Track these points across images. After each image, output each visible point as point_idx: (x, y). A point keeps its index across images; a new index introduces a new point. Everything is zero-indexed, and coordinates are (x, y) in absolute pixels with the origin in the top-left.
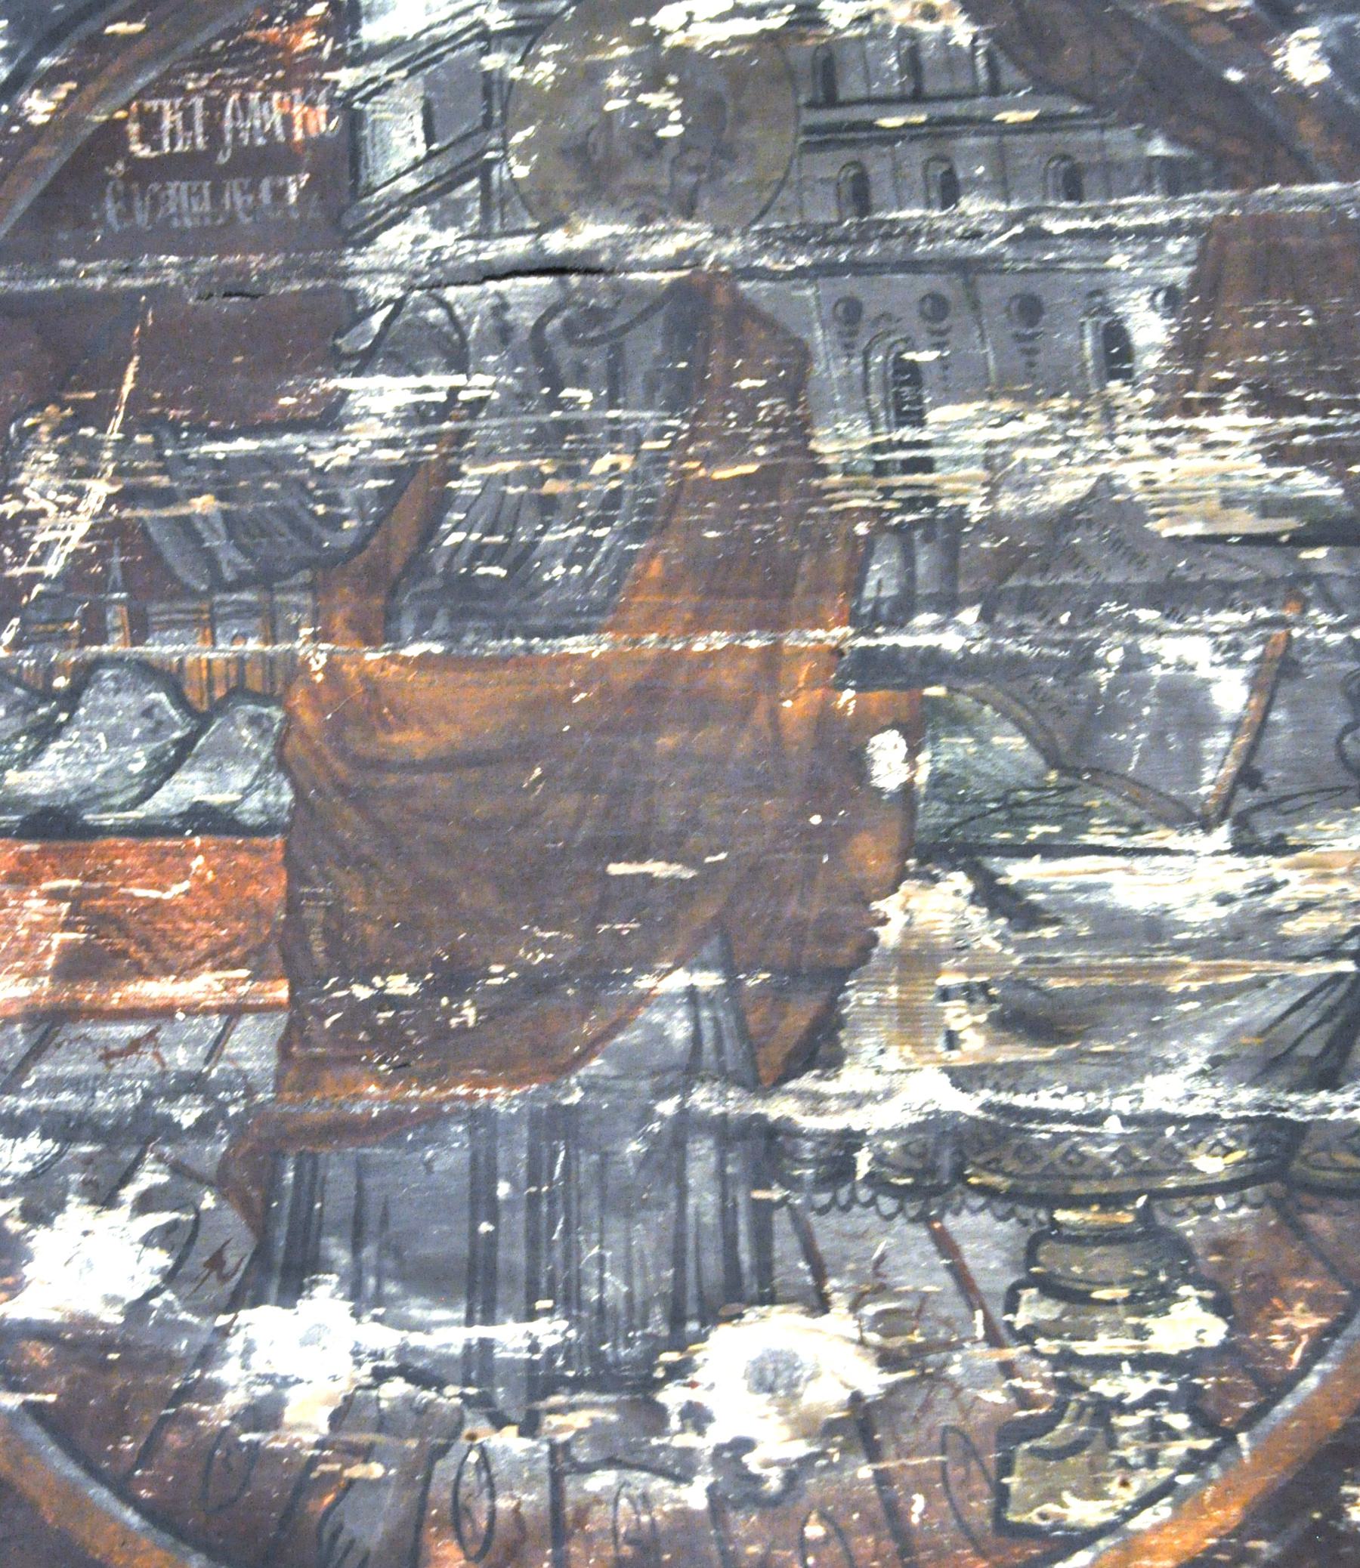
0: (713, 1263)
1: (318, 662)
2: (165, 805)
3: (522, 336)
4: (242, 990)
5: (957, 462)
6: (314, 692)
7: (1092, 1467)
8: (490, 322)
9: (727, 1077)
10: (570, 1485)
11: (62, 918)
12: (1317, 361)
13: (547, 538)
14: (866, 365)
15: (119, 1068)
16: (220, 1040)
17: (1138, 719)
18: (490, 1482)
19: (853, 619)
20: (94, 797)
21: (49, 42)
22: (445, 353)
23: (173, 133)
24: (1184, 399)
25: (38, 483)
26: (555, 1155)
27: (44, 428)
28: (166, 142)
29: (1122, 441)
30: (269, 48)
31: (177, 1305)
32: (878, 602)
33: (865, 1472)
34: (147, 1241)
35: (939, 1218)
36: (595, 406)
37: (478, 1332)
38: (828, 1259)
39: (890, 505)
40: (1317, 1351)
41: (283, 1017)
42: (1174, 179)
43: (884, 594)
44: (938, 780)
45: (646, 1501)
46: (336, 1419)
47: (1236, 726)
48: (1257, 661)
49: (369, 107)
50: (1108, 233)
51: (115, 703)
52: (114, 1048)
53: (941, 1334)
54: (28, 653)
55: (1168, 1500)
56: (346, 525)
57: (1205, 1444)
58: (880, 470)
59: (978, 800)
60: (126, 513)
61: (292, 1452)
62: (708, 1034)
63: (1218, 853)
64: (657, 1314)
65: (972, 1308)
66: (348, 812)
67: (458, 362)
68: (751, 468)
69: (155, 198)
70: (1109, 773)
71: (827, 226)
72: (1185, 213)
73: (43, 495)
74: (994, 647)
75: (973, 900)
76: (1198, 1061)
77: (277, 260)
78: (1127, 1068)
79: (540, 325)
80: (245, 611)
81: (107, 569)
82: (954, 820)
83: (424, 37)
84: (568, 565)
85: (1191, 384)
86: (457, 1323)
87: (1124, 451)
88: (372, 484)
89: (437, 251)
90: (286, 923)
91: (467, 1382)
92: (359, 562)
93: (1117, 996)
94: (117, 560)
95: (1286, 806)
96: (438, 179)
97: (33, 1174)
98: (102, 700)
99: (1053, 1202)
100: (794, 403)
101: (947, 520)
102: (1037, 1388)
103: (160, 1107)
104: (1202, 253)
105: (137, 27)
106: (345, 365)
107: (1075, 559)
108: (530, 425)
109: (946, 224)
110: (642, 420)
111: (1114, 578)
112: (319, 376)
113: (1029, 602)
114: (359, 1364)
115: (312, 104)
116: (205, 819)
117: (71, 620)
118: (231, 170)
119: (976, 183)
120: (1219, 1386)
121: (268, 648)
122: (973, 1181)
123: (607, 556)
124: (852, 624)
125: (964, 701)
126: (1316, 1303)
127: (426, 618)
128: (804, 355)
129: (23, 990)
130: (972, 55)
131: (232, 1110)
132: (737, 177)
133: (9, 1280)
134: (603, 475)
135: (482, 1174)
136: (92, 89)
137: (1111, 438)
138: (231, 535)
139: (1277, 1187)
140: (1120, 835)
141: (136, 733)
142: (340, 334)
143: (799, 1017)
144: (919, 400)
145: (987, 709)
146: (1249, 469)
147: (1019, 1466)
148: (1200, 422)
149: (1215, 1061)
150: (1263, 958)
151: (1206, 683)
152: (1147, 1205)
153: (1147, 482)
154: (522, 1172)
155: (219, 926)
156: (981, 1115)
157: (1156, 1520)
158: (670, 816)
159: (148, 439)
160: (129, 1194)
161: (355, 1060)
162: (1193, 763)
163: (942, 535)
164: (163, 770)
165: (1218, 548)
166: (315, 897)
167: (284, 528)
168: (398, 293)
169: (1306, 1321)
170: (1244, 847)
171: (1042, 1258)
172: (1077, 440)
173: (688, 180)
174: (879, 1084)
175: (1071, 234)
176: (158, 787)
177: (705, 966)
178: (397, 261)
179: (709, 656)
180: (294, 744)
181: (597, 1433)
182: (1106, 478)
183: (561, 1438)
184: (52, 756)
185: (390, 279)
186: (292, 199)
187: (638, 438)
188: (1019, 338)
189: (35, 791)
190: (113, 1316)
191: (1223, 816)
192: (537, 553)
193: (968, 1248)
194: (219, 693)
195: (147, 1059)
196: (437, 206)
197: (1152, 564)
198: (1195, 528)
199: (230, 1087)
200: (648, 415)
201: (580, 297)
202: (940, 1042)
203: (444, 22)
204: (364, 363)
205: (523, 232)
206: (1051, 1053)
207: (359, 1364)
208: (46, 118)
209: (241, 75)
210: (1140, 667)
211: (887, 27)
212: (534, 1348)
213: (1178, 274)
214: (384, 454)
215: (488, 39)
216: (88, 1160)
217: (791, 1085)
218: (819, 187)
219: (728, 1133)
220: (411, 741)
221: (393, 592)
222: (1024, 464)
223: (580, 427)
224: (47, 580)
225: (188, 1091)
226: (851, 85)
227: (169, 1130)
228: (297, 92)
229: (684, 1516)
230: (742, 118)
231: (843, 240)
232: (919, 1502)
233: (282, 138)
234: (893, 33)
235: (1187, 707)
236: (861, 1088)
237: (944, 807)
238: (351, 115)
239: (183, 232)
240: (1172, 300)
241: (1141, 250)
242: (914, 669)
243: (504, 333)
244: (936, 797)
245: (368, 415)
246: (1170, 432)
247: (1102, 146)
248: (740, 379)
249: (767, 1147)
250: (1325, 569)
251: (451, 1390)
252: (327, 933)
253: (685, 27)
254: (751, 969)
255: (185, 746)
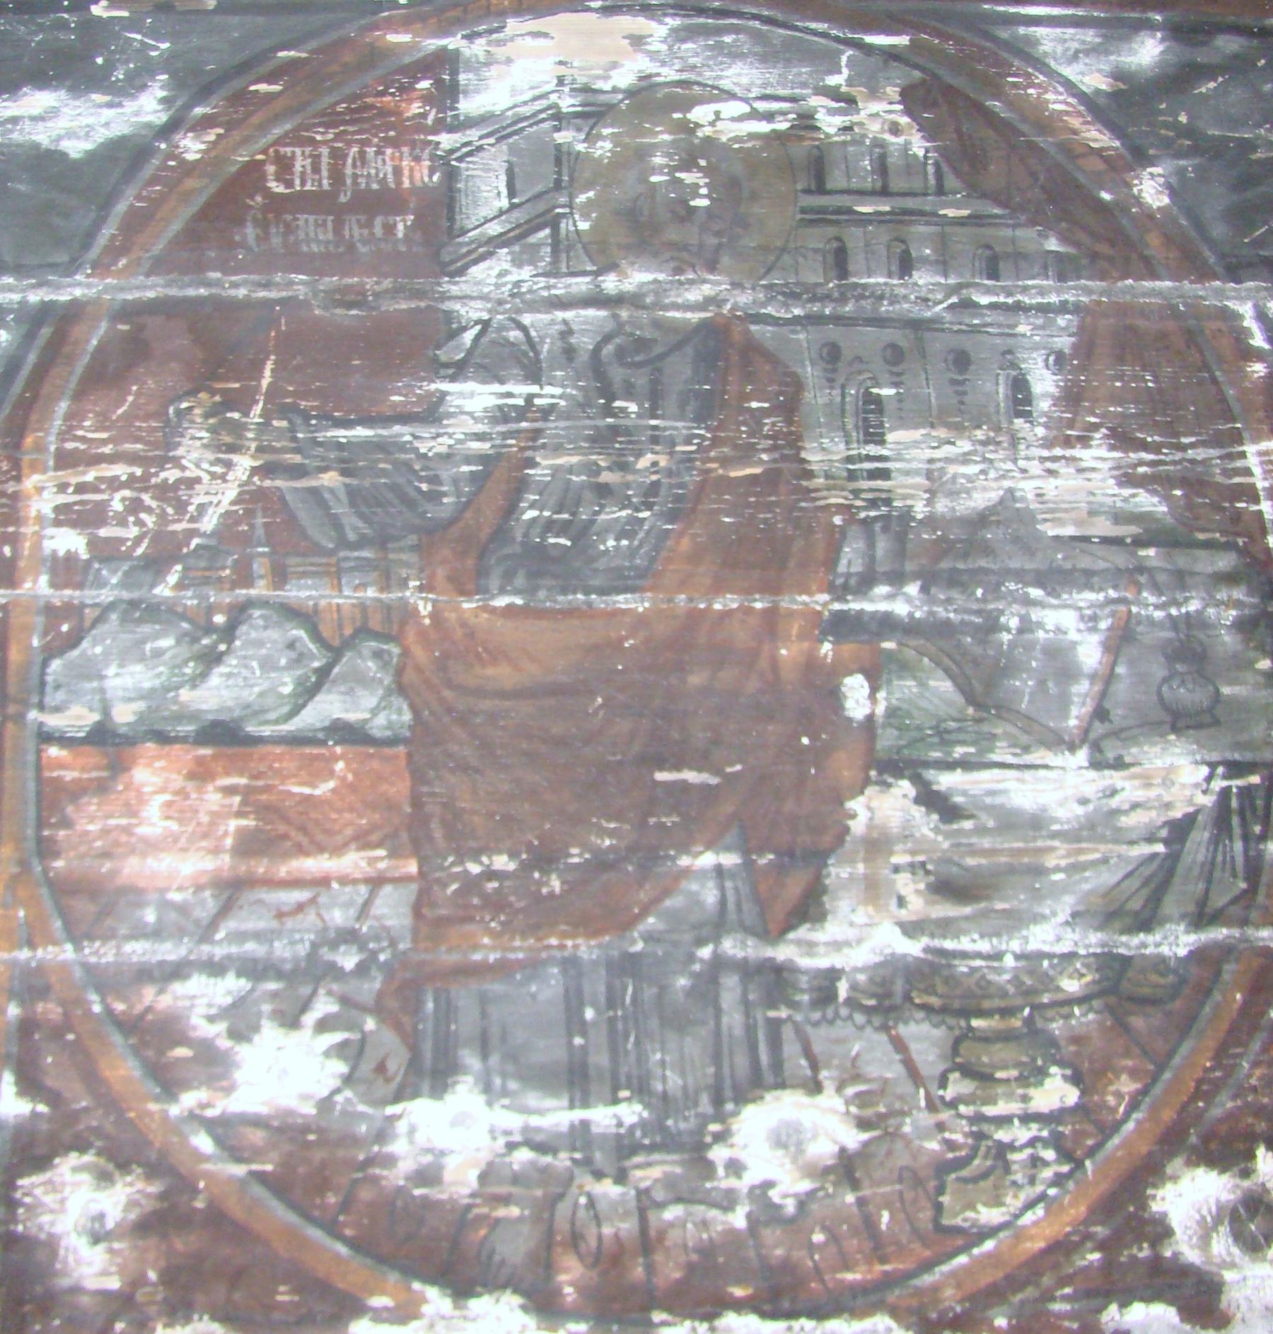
0: (742, 1062)
1: (425, 609)
2: (310, 721)
3: (583, 358)
4: (382, 865)
5: (907, 473)
6: (422, 633)
7: (996, 1187)
8: (559, 344)
9: (749, 931)
10: (652, 1216)
11: (235, 808)
12: (1155, 413)
13: (603, 517)
14: (843, 396)
15: (290, 923)
16: (367, 904)
17: (1029, 670)
18: (596, 1217)
19: (830, 588)
20: (257, 713)
21: (204, 93)
22: (523, 367)
23: (303, 174)
24: (1067, 436)
25: (195, 455)
26: (625, 989)
27: (197, 411)
28: (298, 182)
29: (1021, 463)
30: (384, 112)
31: (355, 1100)
32: (848, 575)
33: (850, 1198)
34: (327, 1054)
35: (895, 1027)
36: (639, 415)
37: (578, 1114)
38: (820, 1058)
39: (858, 503)
40: (1133, 1106)
41: (414, 887)
42: (1063, 269)
43: (853, 570)
44: (892, 712)
45: (705, 1224)
46: (483, 1178)
47: (1093, 677)
48: (1109, 629)
49: (463, 165)
50: (1018, 307)
51: (262, 635)
52: (285, 909)
53: (897, 1106)
54: (190, 593)
55: (1042, 1205)
56: (445, 500)
57: (1065, 1168)
58: (852, 476)
59: (919, 728)
60: (267, 483)
61: (451, 1200)
62: (731, 899)
63: (1081, 768)
64: (705, 1099)
65: (917, 1088)
66: (456, 730)
67: (534, 374)
68: (757, 470)
69: (287, 226)
70: (1009, 710)
71: (817, 285)
72: (1070, 297)
73: (198, 466)
74: (931, 613)
75: (917, 801)
76: (1063, 916)
77: (387, 283)
78: (1016, 920)
79: (596, 351)
80: (363, 566)
81: (252, 526)
82: (902, 743)
83: (510, 113)
84: (617, 539)
85: (1071, 424)
86: (562, 1109)
87: (1024, 471)
88: (465, 469)
89: (517, 284)
90: (411, 815)
91: (574, 1149)
92: (454, 531)
93: (1011, 870)
94: (260, 520)
95: (1123, 735)
96: (518, 226)
97: (234, 1005)
98: (254, 635)
99: (967, 1013)
100: (789, 422)
101: (899, 517)
102: (958, 1137)
103: (326, 954)
104: (1081, 328)
105: (276, 88)
106: (443, 372)
107: (987, 550)
108: (590, 428)
109: (903, 291)
110: (675, 428)
111: (1014, 564)
112: (423, 379)
113: (954, 580)
114: (494, 1139)
115: (417, 159)
116: (348, 734)
117: (224, 568)
118: (351, 207)
119: (925, 261)
120: (1074, 1132)
121: (384, 596)
122: (917, 1001)
123: (648, 532)
124: (829, 592)
125: (910, 654)
126: (1134, 1073)
127: (508, 576)
128: (798, 385)
129: (209, 864)
130: (925, 164)
131: (382, 957)
132: (750, 242)
133: (224, 1083)
134: (646, 469)
135: (573, 1001)
136: (237, 135)
137: (1015, 461)
138: (353, 504)
139: (1112, 1000)
140: (1015, 755)
141: (283, 662)
142: (439, 347)
143: (795, 886)
144: (881, 425)
145: (926, 660)
146: (1108, 489)
147: (948, 1190)
148: (1077, 452)
149: (1074, 915)
150: (1107, 842)
151: (1074, 644)
152: (1031, 1014)
153: (1038, 495)
154: (602, 999)
155: (360, 816)
156: (922, 955)
157: (1034, 1218)
158: (700, 736)
159: (284, 424)
160: (310, 1018)
161: (471, 919)
162: (1064, 702)
163: (895, 527)
164: (308, 691)
165: (1084, 545)
166: (433, 794)
167: (396, 501)
168: (485, 316)
169: (1127, 1085)
170: (1097, 764)
171: (962, 1051)
172: (991, 461)
173: (712, 241)
174: (851, 934)
175: (993, 306)
176: (304, 706)
177: (728, 849)
178: (486, 290)
179: (727, 614)
180: (410, 676)
181: (669, 1182)
182: (1010, 491)
183: (643, 1185)
184: (215, 679)
185: (479, 304)
186: (400, 235)
187: (672, 443)
188: (954, 382)
189: (204, 707)
190: (309, 1109)
191: (1083, 741)
192: (595, 528)
193: (914, 1047)
194: (348, 631)
195: (310, 918)
196: (517, 248)
197: (1040, 555)
198: (1069, 531)
199: (377, 938)
200: (680, 424)
201: (628, 329)
202: (894, 902)
203: (525, 103)
204: (459, 370)
205: (584, 273)
206: (967, 910)
207: (494, 1139)
208: (198, 156)
209: (358, 132)
210: (1031, 631)
211: (864, 136)
212: (620, 1124)
213: (1064, 342)
214: (475, 445)
215: (560, 119)
216: (275, 995)
217: (791, 935)
218: (810, 255)
219: (749, 971)
220: (502, 675)
221: (481, 556)
222: (955, 477)
223: (627, 431)
224: (204, 535)
225: (346, 942)
226: (837, 180)
227: (334, 971)
228: (405, 149)
229: (731, 1232)
230: (754, 197)
231: (827, 297)
232: (886, 1216)
233: (393, 186)
234: (868, 142)
235: (1059, 659)
236: (839, 938)
237: (896, 733)
238: (449, 169)
239: (312, 256)
240: (1060, 361)
241: (1040, 321)
242: (874, 627)
243: (569, 352)
244: (891, 725)
245: (462, 413)
246: (1055, 459)
247: (1013, 241)
248: (749, 401)
249: (776, 981)
250: (1155, 563)
251: (563, 1155)
252: (444, 822)
253: (712, 124)
254: (761, 851)
255: (323, 674)
